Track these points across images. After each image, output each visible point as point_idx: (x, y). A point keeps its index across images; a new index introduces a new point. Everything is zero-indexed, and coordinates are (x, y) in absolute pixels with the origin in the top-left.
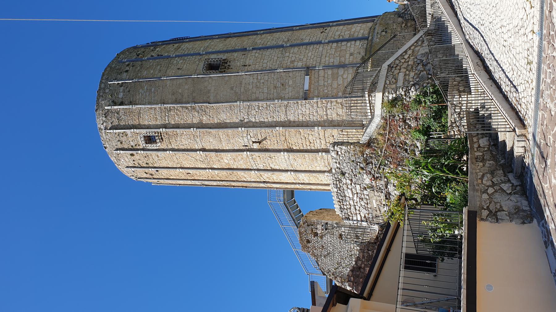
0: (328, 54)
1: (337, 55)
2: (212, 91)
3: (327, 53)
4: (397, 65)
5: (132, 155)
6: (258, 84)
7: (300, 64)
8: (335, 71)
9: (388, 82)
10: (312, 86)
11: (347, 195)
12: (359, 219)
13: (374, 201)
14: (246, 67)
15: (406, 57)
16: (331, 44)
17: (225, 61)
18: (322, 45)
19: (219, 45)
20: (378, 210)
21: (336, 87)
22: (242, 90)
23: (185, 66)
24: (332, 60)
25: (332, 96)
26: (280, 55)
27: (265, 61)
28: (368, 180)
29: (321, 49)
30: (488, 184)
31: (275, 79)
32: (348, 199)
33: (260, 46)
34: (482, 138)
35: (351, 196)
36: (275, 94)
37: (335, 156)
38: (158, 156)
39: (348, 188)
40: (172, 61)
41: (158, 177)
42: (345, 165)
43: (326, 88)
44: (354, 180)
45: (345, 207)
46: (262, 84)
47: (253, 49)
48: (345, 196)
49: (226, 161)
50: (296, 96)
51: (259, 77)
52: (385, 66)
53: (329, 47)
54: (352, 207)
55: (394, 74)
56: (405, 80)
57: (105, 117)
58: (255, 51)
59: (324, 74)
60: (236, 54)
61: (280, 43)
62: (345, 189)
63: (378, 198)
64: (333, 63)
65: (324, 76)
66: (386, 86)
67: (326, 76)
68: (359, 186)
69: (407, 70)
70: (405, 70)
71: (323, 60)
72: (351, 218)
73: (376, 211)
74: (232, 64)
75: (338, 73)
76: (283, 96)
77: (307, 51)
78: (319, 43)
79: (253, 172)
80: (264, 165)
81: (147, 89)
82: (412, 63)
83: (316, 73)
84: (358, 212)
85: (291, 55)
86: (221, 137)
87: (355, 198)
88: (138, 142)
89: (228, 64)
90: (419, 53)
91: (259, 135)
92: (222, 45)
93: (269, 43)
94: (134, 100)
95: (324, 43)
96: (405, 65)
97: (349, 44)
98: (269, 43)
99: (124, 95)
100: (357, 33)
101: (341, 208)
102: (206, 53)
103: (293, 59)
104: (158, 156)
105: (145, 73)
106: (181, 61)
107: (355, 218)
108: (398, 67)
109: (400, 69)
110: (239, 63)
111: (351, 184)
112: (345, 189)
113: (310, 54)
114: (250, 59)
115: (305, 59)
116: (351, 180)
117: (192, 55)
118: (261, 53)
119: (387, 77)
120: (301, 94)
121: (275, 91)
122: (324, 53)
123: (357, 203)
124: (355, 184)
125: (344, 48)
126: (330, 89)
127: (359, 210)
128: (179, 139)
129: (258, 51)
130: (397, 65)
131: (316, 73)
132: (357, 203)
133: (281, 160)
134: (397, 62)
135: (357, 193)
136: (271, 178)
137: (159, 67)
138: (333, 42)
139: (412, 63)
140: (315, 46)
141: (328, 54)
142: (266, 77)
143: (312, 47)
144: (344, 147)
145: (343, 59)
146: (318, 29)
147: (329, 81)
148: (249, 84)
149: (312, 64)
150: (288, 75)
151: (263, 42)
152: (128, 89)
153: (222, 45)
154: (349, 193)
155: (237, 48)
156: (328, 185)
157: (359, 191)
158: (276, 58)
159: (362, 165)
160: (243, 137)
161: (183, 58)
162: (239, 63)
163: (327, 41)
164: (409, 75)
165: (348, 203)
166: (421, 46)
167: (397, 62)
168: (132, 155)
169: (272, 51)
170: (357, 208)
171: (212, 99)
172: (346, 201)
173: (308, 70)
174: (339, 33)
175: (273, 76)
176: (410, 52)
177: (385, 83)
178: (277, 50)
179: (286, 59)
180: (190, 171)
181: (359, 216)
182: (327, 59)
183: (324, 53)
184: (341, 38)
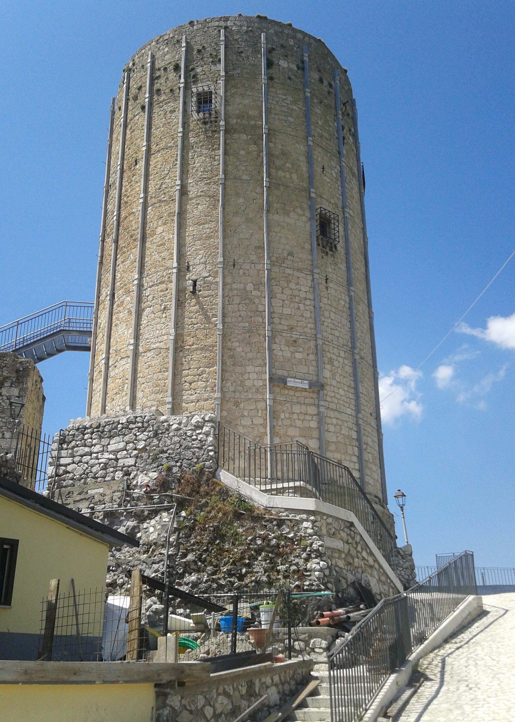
0: (340, 423)
1: (339, 439)
2: (287, 220)
3: (343, 421)
4: (353, 538)
5: (177, 68)
6: (297, 299)
7: (327, 374)
8: (315, 434)
9: (330, 520)
10: (291, 393)
11: (112, 442)
12: (63, 461)
13: (101, 490)
14: (324, 282)
15: (364, 554)
16: (355, 428)
17: (333, 248)
18: (354, 413)
19: (355, 244)
20: (82, 497)
21: (289, 433)
22: (288, 271)
23: (328, 180)
24: (332, 428)
25: (274, 427)
26: (341, 340)
27: (333, 316)
28: (146, 480)
29: (349, 411)
30: (217, 705)
31: (305, 330)
32: (105, 441)
33: (355, 311)
34: (279, 693)
35: (111, 448)
36: (279, 327)
37: (194, 421)
38: (172, 112)
39: (127, 443)
40: (335, 159)
41: (130, 108)
42: (176, 439)
43: (287, 416)
44: (145, 455)
45: (86, 437)
46: (296, 305)
47: (350, 297)
48: (111, 437)
49: (160, 230)
50: (276, 364)
51: (308, 302)
52: (352, 518)
53: (350, 425)
54: (87, 449)
55: (341, 532)
56: (333, 550)
57: (247, 32)
58: (348, 301)
59: (310, 415)
60: (343, 266)
61: (358, 345)
62: (126, 438)
63: (107, 499)
64: (328, 431)
65: (306, 414)
66: (325, 517)
67: (308, 418)
68: (133, 463)
69: (346, 555)
70: (346, 551)
71: (332, 414)
72: (65, 446)
73: (80, 494)
74: (330, 259)
75: (312, 438)
76: (277, 340)
77: (346, 389)
78: (358, 410)
79: (136, 276)
80: (150, 298)
81: (292, 110)
82: (356, 564)
83: (312, 401)
84: (77, 459)
85: (341, 360)
86: (206, 226)
87: (106, 455)
88: (202, 81)
89: (330, 253)
90: (369, 578)
91: (207, 293)
92: (356, 246)
93: (358, 324)
94: (275, 85)
95: (357, 417)
96: (353, 552)
97: (355, 459)
98: (358, 324)
99: (284, 68)
100: (369, 473)
101: (85, 428)
102: (345, 218)
103: (336, 363)
104: (172, 112)
105: (318, 111)
106: (334, 175)
107: (64, 453)
108: (350, 541)
109: (347, 543)
110: (330, 270)
111: (135, 449)
112: (126, 438)
113: (341, 392)
114: (336, 290)
115: (334, 383)
116: (144, 449)
117: (343, 194)
118: (345, 310)
119: (337, 519)
120: (280, 373)
121: (286, 328)
122: (344, 417)
123: (97, 458)
124: (137, 457)
125: (350, 450)
126: (287, 422)
127: (80, 461)
128: (205, 151)
129: (347, 306)
130: (353, 538)
131: (312, 401)
132: (97, 458)
133: (159, 331)
134: (358, 538)
135: (117, 460)
136: (121, 309)
137: (326, 135)
138: (358, 432)
139: (356, 564)
140: (353, 402)
141: (340, 423)
142: (308, 314)
143: (352, 396)
144: (210, 439)
145: (333, 447)
146: (375, 410)
147: (298, 423)
148: (297, 284)
149: (326, 395)
150: (311, 352)
151: (359, 314)
152: (292, 77)
153: (356, 246)
154: (116, 444)
155: (353, 271)
156: (104, 411)
157: (121, 463)
158: (337, 333)
159: (175, 470)
160: (205, 263)
161: (339, 178)
162: (330, 270)
163: (361, 422)
164: (339, 558)
165: (94, 442)
166: (379, 580)
167: (358, 538)
168: (177, 68)
169: (348, 329)
170: (86, 459)
171: (271, 216)
172: (101, 437)
173: (318, 387)
174: (370, 443)
175: (309, 325)
176: (371, 561)
177: (329, 516)
178: (348, 337)
179: (336, 351)
180: (142, 164)
181: (69, 460)
182: (334, 421)
183: (344, 417)
184: (364, 446)
